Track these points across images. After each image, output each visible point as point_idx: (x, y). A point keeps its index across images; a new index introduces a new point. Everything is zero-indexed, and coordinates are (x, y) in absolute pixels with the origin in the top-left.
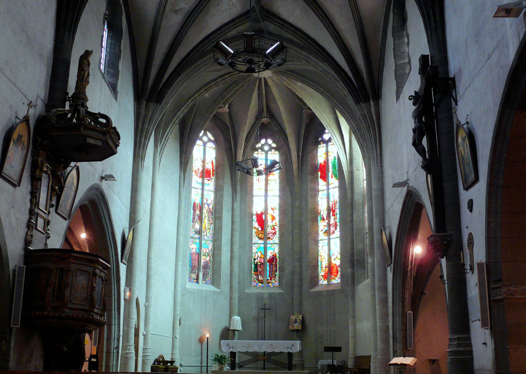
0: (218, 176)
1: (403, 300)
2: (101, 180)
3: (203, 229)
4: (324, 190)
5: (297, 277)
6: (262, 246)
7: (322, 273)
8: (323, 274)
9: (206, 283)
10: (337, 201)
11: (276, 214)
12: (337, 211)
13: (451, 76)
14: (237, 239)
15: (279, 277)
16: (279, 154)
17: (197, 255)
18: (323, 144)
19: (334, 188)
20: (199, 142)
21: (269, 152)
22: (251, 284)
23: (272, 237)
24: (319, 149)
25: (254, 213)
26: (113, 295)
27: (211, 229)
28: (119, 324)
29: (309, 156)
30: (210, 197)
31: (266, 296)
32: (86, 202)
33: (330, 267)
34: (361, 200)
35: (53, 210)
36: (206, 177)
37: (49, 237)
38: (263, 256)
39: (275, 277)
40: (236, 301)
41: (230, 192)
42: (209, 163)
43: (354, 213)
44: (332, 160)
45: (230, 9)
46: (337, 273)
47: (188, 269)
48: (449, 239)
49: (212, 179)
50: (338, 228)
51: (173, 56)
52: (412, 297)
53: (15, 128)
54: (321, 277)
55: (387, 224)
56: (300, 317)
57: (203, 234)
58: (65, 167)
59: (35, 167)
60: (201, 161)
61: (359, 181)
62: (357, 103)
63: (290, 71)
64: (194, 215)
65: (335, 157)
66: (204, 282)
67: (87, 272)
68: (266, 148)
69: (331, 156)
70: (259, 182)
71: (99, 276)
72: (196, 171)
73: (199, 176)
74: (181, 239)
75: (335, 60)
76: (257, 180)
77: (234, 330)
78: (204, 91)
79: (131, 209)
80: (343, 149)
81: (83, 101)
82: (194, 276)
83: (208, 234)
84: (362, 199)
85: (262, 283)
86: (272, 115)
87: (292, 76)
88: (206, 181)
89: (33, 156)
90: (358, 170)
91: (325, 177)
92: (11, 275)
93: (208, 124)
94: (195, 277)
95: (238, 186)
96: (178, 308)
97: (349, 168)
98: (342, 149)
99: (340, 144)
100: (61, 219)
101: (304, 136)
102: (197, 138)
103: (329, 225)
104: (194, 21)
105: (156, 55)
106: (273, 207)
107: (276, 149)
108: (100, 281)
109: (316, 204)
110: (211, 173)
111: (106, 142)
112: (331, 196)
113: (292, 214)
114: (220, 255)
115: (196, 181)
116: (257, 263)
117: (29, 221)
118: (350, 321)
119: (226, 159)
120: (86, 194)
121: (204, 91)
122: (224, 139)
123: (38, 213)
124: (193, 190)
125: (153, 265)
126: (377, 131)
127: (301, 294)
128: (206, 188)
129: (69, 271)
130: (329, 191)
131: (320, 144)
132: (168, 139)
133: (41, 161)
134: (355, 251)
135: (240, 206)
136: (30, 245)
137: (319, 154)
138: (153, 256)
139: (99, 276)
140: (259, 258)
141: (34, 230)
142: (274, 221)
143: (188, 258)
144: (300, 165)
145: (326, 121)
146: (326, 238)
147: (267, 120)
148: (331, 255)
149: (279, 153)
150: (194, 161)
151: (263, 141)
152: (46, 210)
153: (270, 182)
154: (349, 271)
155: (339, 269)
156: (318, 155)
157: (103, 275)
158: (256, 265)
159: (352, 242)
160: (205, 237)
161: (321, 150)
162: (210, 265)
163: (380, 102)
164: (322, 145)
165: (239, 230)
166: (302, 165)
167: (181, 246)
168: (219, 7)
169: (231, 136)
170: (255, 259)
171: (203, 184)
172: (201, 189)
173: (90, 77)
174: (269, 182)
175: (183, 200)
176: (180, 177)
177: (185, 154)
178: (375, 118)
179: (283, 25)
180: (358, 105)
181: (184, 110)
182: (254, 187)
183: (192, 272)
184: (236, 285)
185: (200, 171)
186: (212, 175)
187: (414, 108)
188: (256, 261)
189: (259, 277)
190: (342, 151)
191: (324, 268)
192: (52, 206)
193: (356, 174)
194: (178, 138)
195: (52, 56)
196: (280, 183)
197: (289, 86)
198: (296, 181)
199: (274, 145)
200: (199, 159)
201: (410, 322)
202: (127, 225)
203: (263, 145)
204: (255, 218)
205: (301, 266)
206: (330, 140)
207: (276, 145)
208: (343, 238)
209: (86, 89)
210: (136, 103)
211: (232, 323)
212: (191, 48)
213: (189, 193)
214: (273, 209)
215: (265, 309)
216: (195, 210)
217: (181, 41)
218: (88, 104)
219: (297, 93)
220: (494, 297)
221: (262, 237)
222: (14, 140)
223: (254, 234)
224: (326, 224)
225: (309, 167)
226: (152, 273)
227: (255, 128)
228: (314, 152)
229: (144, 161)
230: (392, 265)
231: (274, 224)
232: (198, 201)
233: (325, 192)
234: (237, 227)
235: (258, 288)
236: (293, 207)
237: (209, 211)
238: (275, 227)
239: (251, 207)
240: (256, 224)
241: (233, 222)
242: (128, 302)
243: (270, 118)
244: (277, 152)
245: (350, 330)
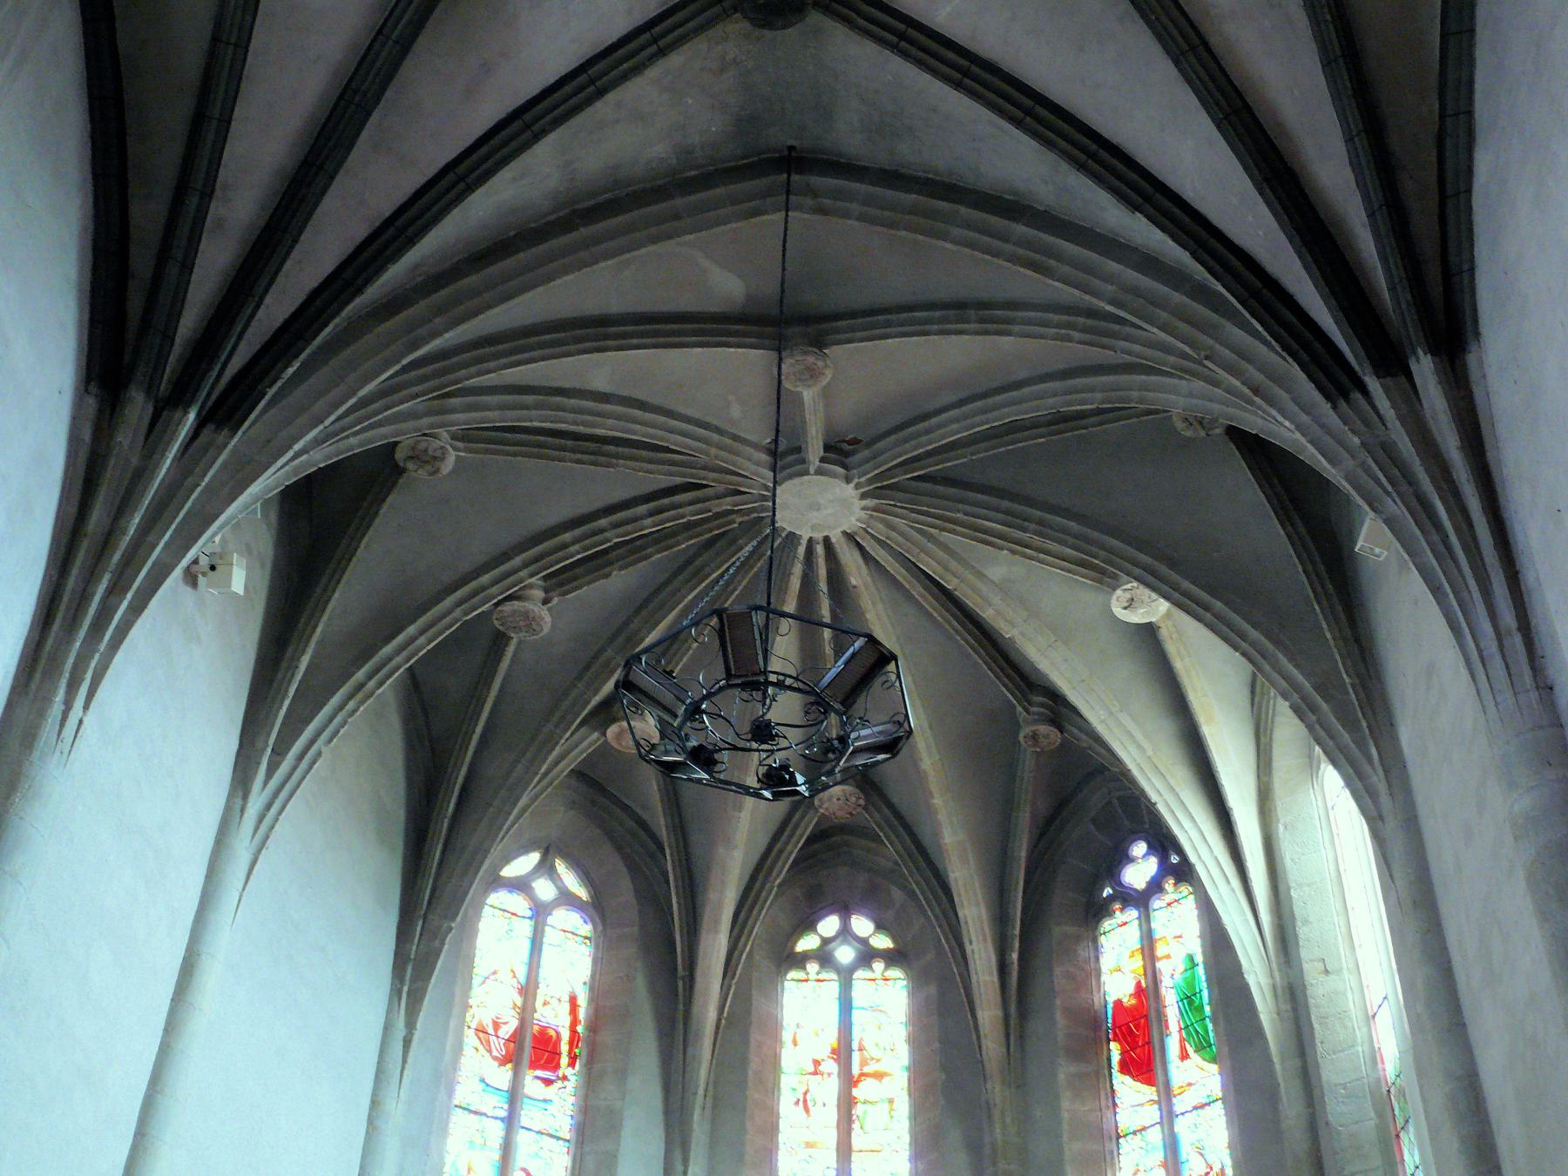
0: (597, 1066)
4: (1144, 1129)
10: (1222, 1170)
16: (905, 982)
18: (1122, 910)
19: (1203, 1106)
21: (860, 974)
24: (1103, 939)
29: (1058, 971)
34: (1371, 1123)
36: (534, 1065)
42: (554, 1002)
44: (1177, 976)
49: (565, 1078)
60: (516, 985)
61: (1345, 1027)
62: (1334, 392)
65: (1191, 958)
68: (845, 954)
69: (1168, 957)
70: (806, 1109)
72: (480, 1030)
73: (495, 1053)
75: (1191, 207)
76: (797, 1103)
78: (526, 565)
80: (1236, 883)
84: (1372, 1114)
87: (961, 501)
88: (532, 1083)
90: (1327, 972)
91: (1143, 1065)
95: (696, 1117)
97: (1277, 974)
98: (1228, 882)
99: (1216, 858)
101: (1027, 882)
107: (893, 958)
110: (564, 1048)
112: (1186, 1151)
115: (478, 1079)
119: (641, 983)
121: (526, 565)
122: (639, 894)
124: (458, 1120)
128: (529, 1115)
130: (1176, 1129)
131: (1110, 914)
132: (314, 762)
137: (1107, 962)
145: (1139, 746)
147: (843, 790)
149: (909, 977)
150: (476, 981)
151: (829, 925)
153: (865, 1112)
156: (1104, 968)
163: (1471, 359)
164: (1119, 917)
166: (1023, 1014)
169: (671, 882)
171: (514, 1096)
172: (502, 1119)
174: (858, 1110)
176: (387, 1028)
177: (425, 918)
180: (1342, 404)
182: (782, 1138)
185: (506, 1031)
186: (564, 1060)
190: (1233, 890)
193: (1321, 992)
194: (399, 816)
197: (949, 577)
198: (996, 1091)
199: (883, 942)
200: (505, 975)
207: (894, 939)
210: (91, 403)
212: (431, 172)
225: (1061, 1021)
227: (787, 843)
228: (1084, 952)
229: (86, 707)
233: (1155, 1136)
244: (896, 973)
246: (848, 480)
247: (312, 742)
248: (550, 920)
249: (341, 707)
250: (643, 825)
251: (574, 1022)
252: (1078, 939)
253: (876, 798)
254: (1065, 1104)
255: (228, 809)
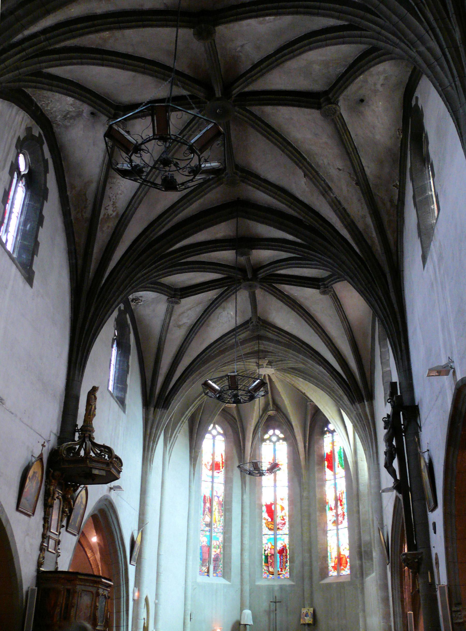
1: (402, 600)
2: (110, 491)
3: (214, 522)
5: (307, 568)
6: (273, 536)
7: (331, 563)
8: (333, 565)
9: (217, 576)
11: (286, 504)
12: (344, 501)
13: (417, 404)
14: (247, 530)
15: (290, 568)
17: (208, 548)
20: (208, 436)
22: (262, 576)
23: (281, 528)
24: (325, 439)
25: (264, 503)
26: (122, 597)
27: (222, 521)
28: (127, 626)
30: (220, 489)
31: (276, 588)
32: (96, 512)
33: (340, 559)
35: (63, 530)
36: (216, 470)
37: (60, 555)
38: (273, 547)
39: (285, 568)
40: (247, 594)
41: (240, 483)
43: (360, 504)
45: (229, 321)
46: (347, 564)
47: (199, 562)
48: (420, 557)
50: (346, 517)
51: (178, 365)
52: (412, 596)
53: (32, 466)
54: (330, 568)
55: (385, 524)
56: (311, 610)
57: (213, 526)
58: (75, 490)
59: (48, 495)
63: (292, 368)
64: (204, 508)
66: (215, 575)
67: (92, 592)
71: (102, 595)
72: (205, 465)
74: (191, 533)
77: (245, 625)
79: (140, 511)
80: (347, 440)
81: (90, 433)
82: (205, 569)
83: (218, 526)
85: (273, 574)
86: (278, 408)
88: (215, 473)
89: (46, 486)
91: (331, 467)
92: (24, 597)
93: (216, 418)
94: (206, 571)
96: (189, 602)
100: (71, 536)
102: (206, 431)
103: (337, 515)
104: (196, 334)
105: (163, 362)
106: (282, 498)
107: (284, 439)
108: (104, 599)
109: (323, 494)
110: (221, 465)
111: (110, 471)
113: (301, 505)
114: (230, 547)
116: (267, 554)
117: (42, 545)
118: (361, 615)
119: (235, 451)
120: (95, 508)
123: (49, 536)
125: (163, 563)
126: (372, 430)
127: (311, 586)
129: (75, 592)
131: (326, 434)
133: (53, 490)
134: (363, 542)
135: (250, 497)
136: (42, 566)
138: (162, 553)
139: (102, 595)
140: (269, 550)
141: (46, 552)
142: (283, 512)
143: (199, 551)
144: (307, 455)
146: (335, 528)
148: (340, 546)
151: (271, 432)
152: (57, 531)
154: (358, 562)
155: (348, 560)
157: (106, 593)
158: (267, 557)
159: (359, 533)
160: (216, 529)
161: (327, 438)
162: (221, 557)
163: (374, 402)
165: (248, 522)
166: (309, 455)
167: (191, 540)
168: (219, 320)
170: (265, 550)
171: (213, 477)
173: (96, 410)
175: (193, 493)
176: (190, 471)
178: (370, 418)
179: (279, 333)
181: (192, 409)
183: (202, 565)
184: (247, 577)
185: (210, 464)
187: (386, 431)
188: (266, 552)
189: (270, 569)
191: (334, 559)
192: (63, 526)
195: (64, 392)
196: (289, 473)
199: (282, 436)
201: (411, 623)
202: (136, 527)
203: (271, 436)
204: (264, 509)
205: (311, 557)
206: (334, 431)
208: (350, 528)
209: (93, 422)
210: (144, 410)
211: (242, 617)
213: (199, 487)
214: (282, 499)
215: (275, 602)
216: (205, 503)
217: (185, 352)
218: (95, 435)
219: (300, 388)
220: (456, 620)
221: (272, 528)
222: (29, 478)
223: (264, 525)
224: (334, 514)
225: (316, 457)
226: (162, 570)
228: (321, 442)
230: (390, 564)
231: (284, 515)
232: (208, 495)
233: (333, 482)
234: (247, 518)
235: (269, 580)
236: (301, 497)
237: (220, 504)
238: (285, 518)
239: (260, 498)
240: (265, 515)
241: (242, 514)
242: (137, 602)
243: (276, 410)
244: (285, 443)
245: (361, 624)
246: (272, 368)
247: (176, 434)
248: (216, 438)
249: (180, 426)
250: (233, 416)
251: (222, 459)
252: (320, 439)
253: (280, 411)
254: (316, 475)
255: (164, 450)
